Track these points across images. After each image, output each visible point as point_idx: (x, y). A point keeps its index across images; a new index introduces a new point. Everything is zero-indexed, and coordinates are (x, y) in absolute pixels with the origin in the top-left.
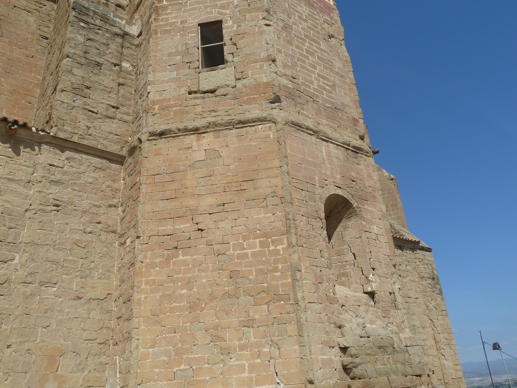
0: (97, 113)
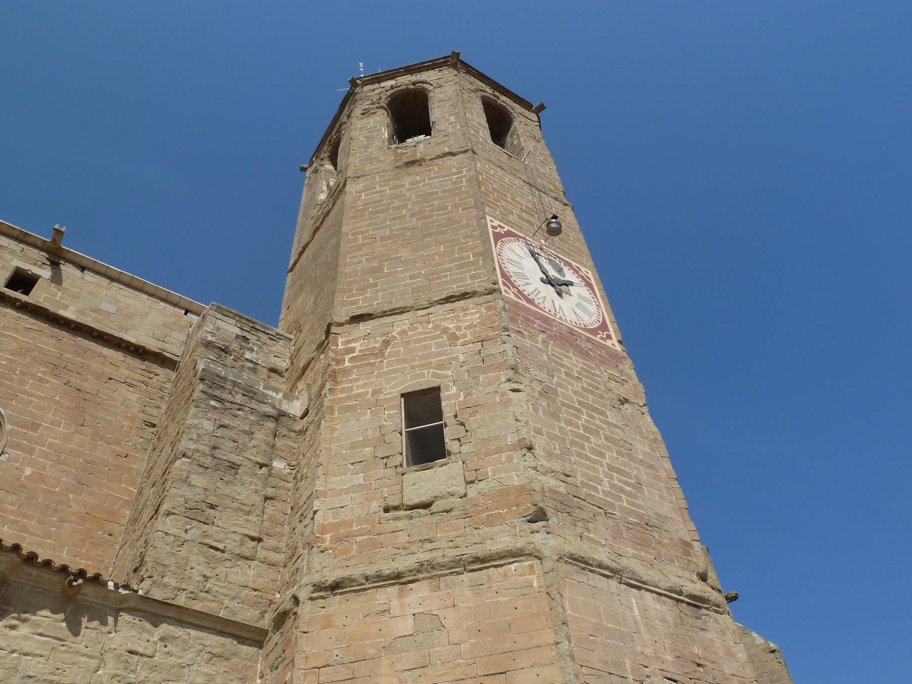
0: (223, 551)
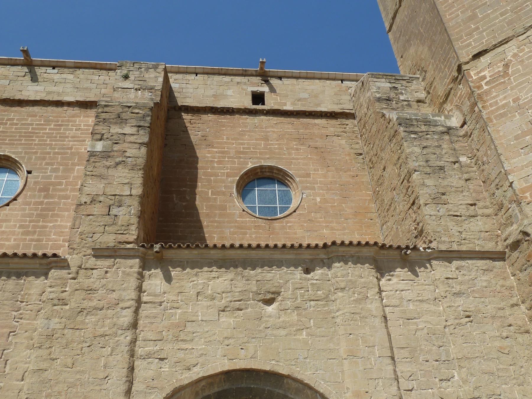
0: (461, 216)
